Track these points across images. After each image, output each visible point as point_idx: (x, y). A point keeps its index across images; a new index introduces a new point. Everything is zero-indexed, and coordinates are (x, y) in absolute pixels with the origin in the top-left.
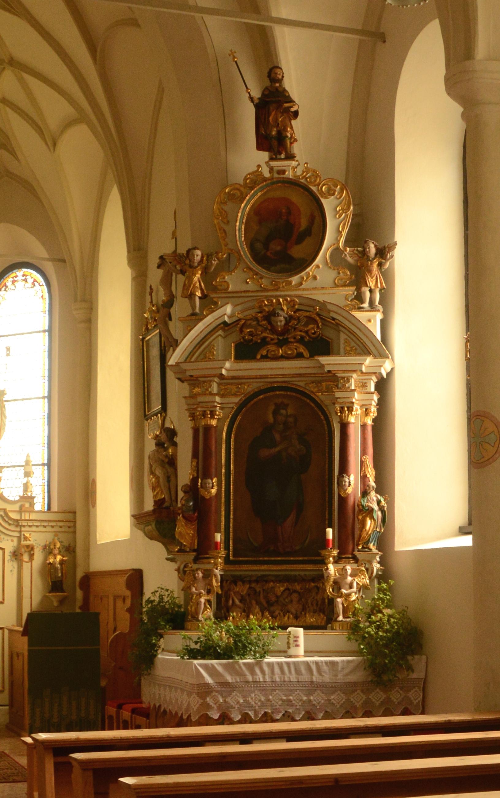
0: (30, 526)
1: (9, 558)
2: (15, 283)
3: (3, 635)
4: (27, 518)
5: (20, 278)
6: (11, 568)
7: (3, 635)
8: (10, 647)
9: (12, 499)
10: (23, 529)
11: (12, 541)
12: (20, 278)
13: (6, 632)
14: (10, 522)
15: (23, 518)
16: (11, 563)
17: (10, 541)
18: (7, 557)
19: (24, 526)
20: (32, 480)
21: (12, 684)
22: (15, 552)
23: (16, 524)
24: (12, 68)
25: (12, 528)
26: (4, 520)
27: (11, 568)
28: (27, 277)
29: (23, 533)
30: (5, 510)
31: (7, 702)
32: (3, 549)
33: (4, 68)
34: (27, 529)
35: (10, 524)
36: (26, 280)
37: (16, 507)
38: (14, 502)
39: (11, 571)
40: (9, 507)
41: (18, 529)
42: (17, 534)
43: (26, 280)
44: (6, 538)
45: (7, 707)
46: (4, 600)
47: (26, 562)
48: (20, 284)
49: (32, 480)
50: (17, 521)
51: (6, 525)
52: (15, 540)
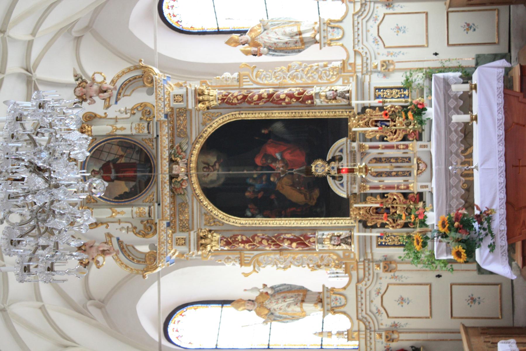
0: (369, 269)
1: (391, 9)
2: (175, 14)
3: (452, 11)
4: (361, 67)
5: (171, 11)
6: (399, 8)
7: (452, 11)
8: (463, 6)
9: (345, 7)
10: (369, 70)
11: (377, 7)
12: (171, 11)
13: (450, 9)
14: (363, 10)
15: (361, 70)
16: (395, 8)
17: (378, 10)
18: (391, 11)
19: (367, 69)
20: (334, 337)
21: (492, 4)
22: (386, 5)
23: (364, 6)
24: (8, 30)
25: (367, 8)
26: (361, 15)
27: (399, 8)
28: (170, 6)
29: (372, 70)
30: (354, 15)
31: (507, 7)
32: (385, 15)
33: (8, 36)
34: (369, 67)
35: (365, 10)
36: (172, 7)
37: (351, 5)
38: (347, 6)
39: (403, 54)
40: (351, 12)
41: (368, 3)
42: (372, 4)
43: (172, 7)
44: (375, 12)
45: (511, 6)
46: (424, 12)
47: (395, 66)
48: (175, 11)
49: (334, 337)
50: (362, 5)
51: (365, 13)
52: (376, 5)
